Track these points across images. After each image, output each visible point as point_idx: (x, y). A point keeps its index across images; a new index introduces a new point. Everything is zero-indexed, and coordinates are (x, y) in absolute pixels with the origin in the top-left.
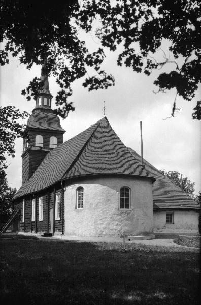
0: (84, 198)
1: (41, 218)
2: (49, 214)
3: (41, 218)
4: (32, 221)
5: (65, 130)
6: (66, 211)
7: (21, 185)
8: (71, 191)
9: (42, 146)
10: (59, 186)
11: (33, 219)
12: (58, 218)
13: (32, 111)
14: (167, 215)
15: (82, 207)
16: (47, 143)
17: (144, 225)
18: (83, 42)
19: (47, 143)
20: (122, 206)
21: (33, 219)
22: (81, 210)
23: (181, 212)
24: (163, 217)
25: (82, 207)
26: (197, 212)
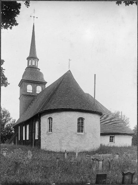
0: (53, 123)
1: (28, 139)
2: (32, 134)
3: (28, 139)
4: (27, 139)
5: (47, 81)
6: (42, 133)
7: (19, 117)
8: (44, 120)
9: (31, 92)
10: (37, 118)
11: (24, 139)
12: (37, 138)
13: (71, 71)
14: (110, 137)
15: (52, 131)
16: (34, 89)
17: (94, 144)
18: (11, 28)
19: (34, 89)
20: (79, 131)
21: (24, 139)
22: (51, 133)
23: (128, 136)
24: (108, 138)
25: (52, 131)
26: (131, 136)
